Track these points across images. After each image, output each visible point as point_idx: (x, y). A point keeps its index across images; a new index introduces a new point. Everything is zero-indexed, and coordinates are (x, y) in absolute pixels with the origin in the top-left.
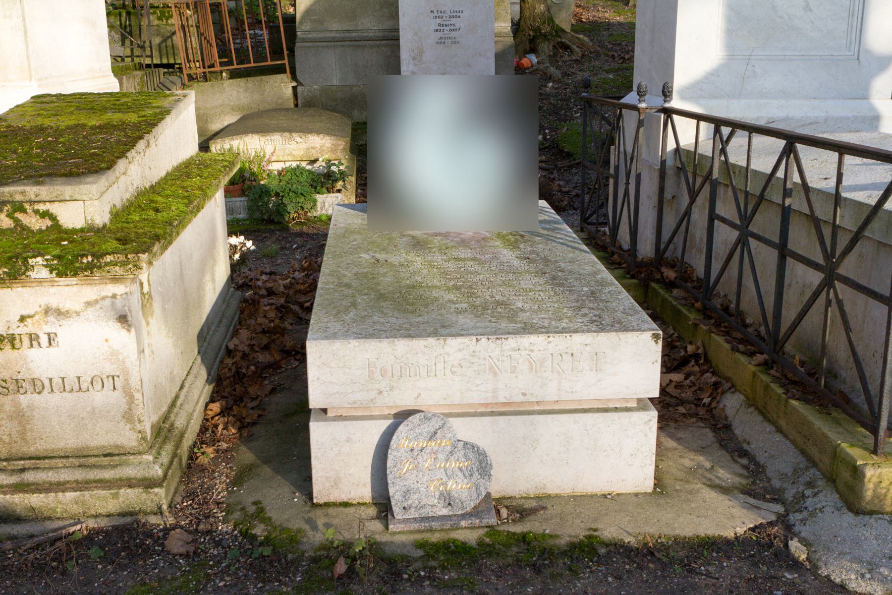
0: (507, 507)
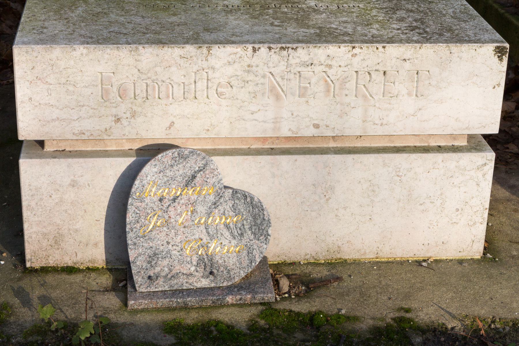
0: (288, 276)
